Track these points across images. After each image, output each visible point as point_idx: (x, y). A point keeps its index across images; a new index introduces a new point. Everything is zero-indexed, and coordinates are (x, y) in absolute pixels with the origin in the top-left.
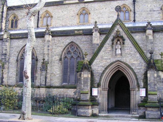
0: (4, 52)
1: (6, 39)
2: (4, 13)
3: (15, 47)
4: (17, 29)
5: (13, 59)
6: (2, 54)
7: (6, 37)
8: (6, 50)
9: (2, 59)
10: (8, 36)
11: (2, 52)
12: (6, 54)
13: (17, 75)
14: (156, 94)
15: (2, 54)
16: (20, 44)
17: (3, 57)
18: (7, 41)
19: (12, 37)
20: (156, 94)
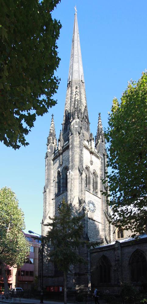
0: (117, 258)
1: (117, 247)
2: (111, 228)
3: (126, 253)
4: (124, 238)
5: (104, 240)
6: (116, 261)
7: (117, 246)
8: (118, 256)
9: (116, 264)
10: (119, 245)
11: (116, 259)
12: (118, 260)
13: (55, 187)
14: (49, 211)
15: (116, 261)
16: (130, 250)
17: (117, 263)
18: (118, 249)
19: (122, 245)
20: (49, 211)
